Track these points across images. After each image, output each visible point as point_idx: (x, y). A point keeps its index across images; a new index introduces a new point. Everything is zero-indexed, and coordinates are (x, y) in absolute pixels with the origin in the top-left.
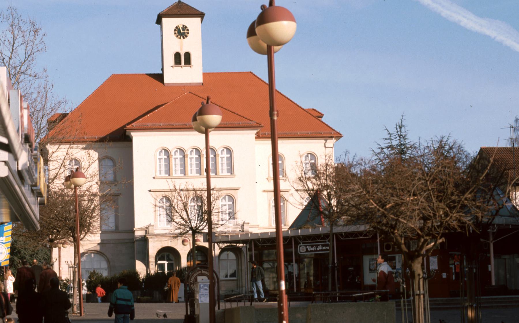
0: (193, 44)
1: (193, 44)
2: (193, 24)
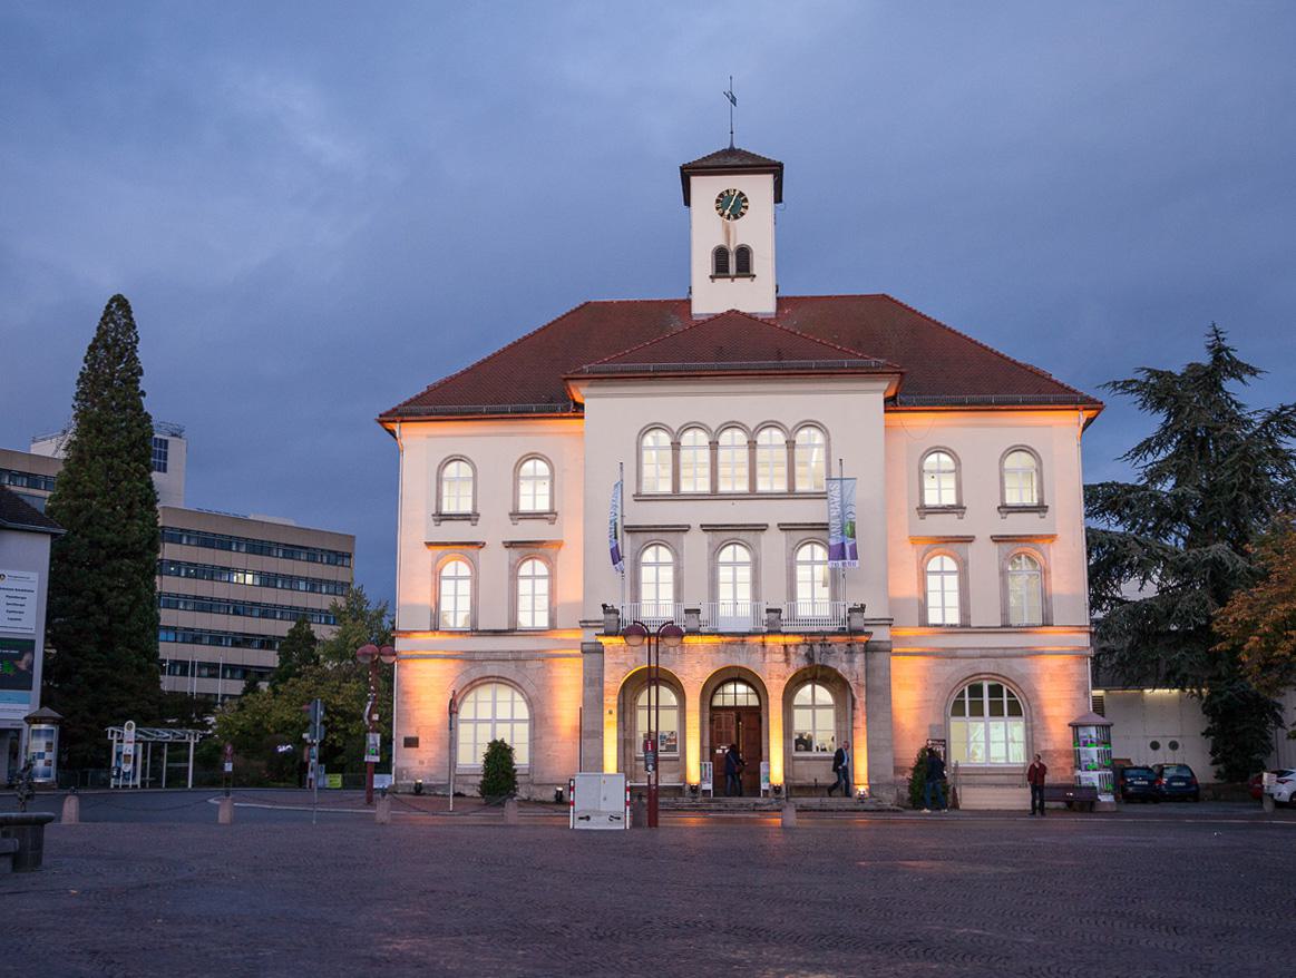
0: (757, 230)
1: (757, 230)
2: (757, 188)
